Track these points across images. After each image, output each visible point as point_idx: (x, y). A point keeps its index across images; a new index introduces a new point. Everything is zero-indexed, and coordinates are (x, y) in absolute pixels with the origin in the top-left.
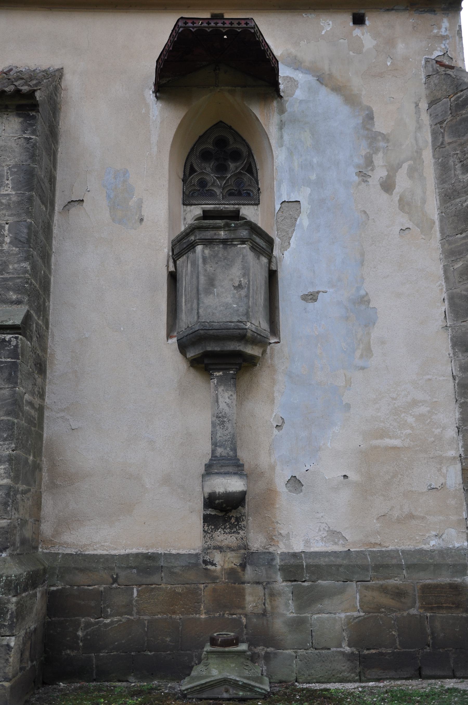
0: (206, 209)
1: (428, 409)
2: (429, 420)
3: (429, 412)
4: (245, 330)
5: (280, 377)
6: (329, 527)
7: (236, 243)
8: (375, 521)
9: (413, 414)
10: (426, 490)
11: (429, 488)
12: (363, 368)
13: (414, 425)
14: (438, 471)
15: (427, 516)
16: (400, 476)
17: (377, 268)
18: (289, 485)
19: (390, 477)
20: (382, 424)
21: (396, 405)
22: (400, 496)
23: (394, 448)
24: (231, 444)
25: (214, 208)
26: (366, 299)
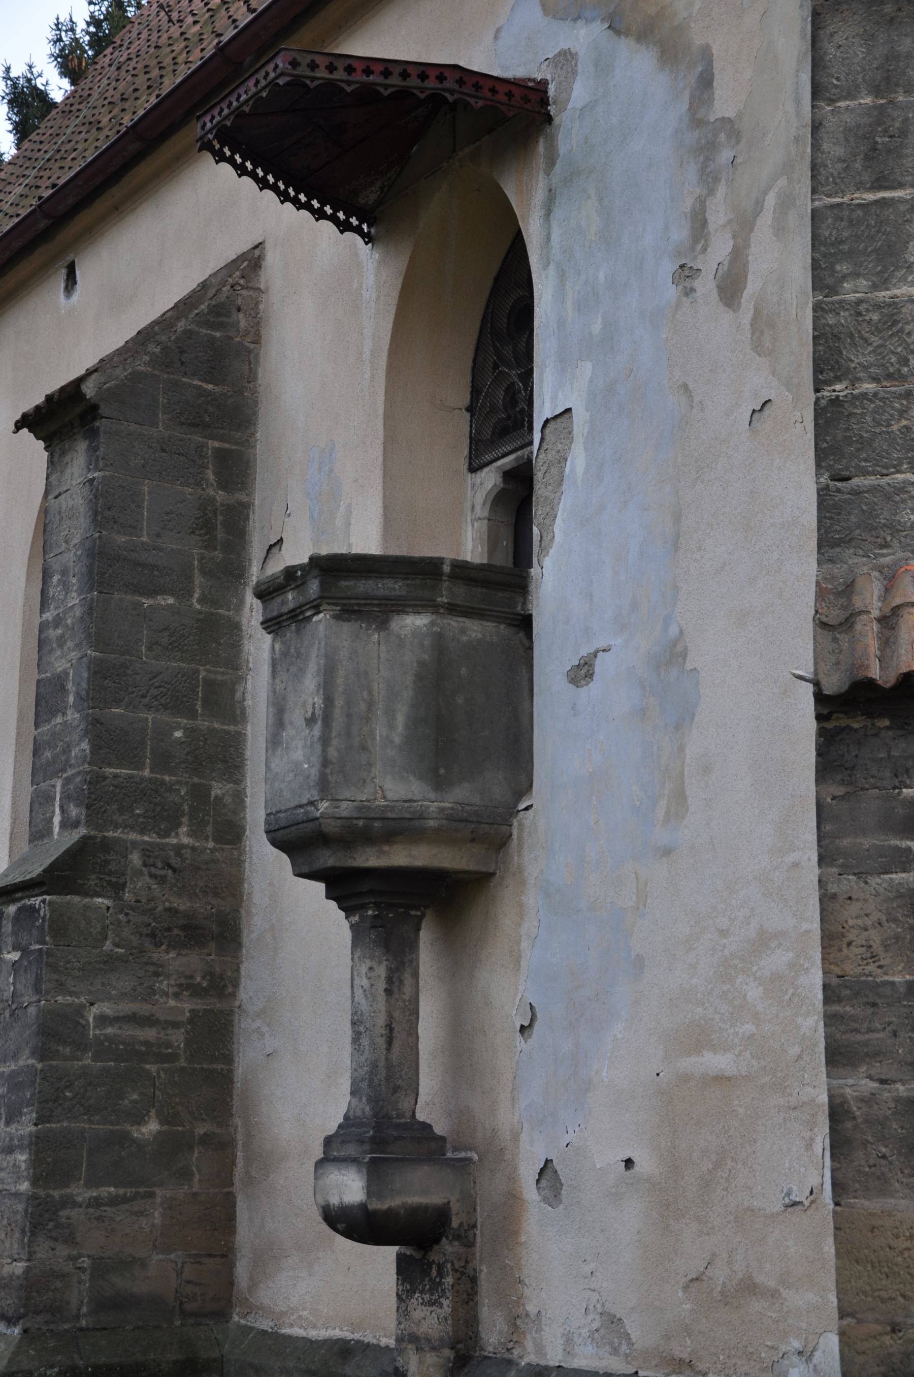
0: (508, 467)
1: (791, 955)
2: (790, 992)
3: (792, 965)
4: (317, 822)
5: (532, 899)
6: (603, 1305)
7: (308, 614)
8: (680, 1294)
9: (758, 974)
10: (778, 1207)
11: (787, 1200)
12: (667, 852)
13: (760, 1008)
14: (807, 1150)
15: (782, 1290)
16: (730, 1163)
17: (705, 550)
18: (544, 1183)
19: (710, 1167)
20: (700, 1010)
21: (726, 952)
22: (729, 1222)
23: (721, 1079)
24: (370, 1086)
25: (516, 459)
26: (679, 648)
